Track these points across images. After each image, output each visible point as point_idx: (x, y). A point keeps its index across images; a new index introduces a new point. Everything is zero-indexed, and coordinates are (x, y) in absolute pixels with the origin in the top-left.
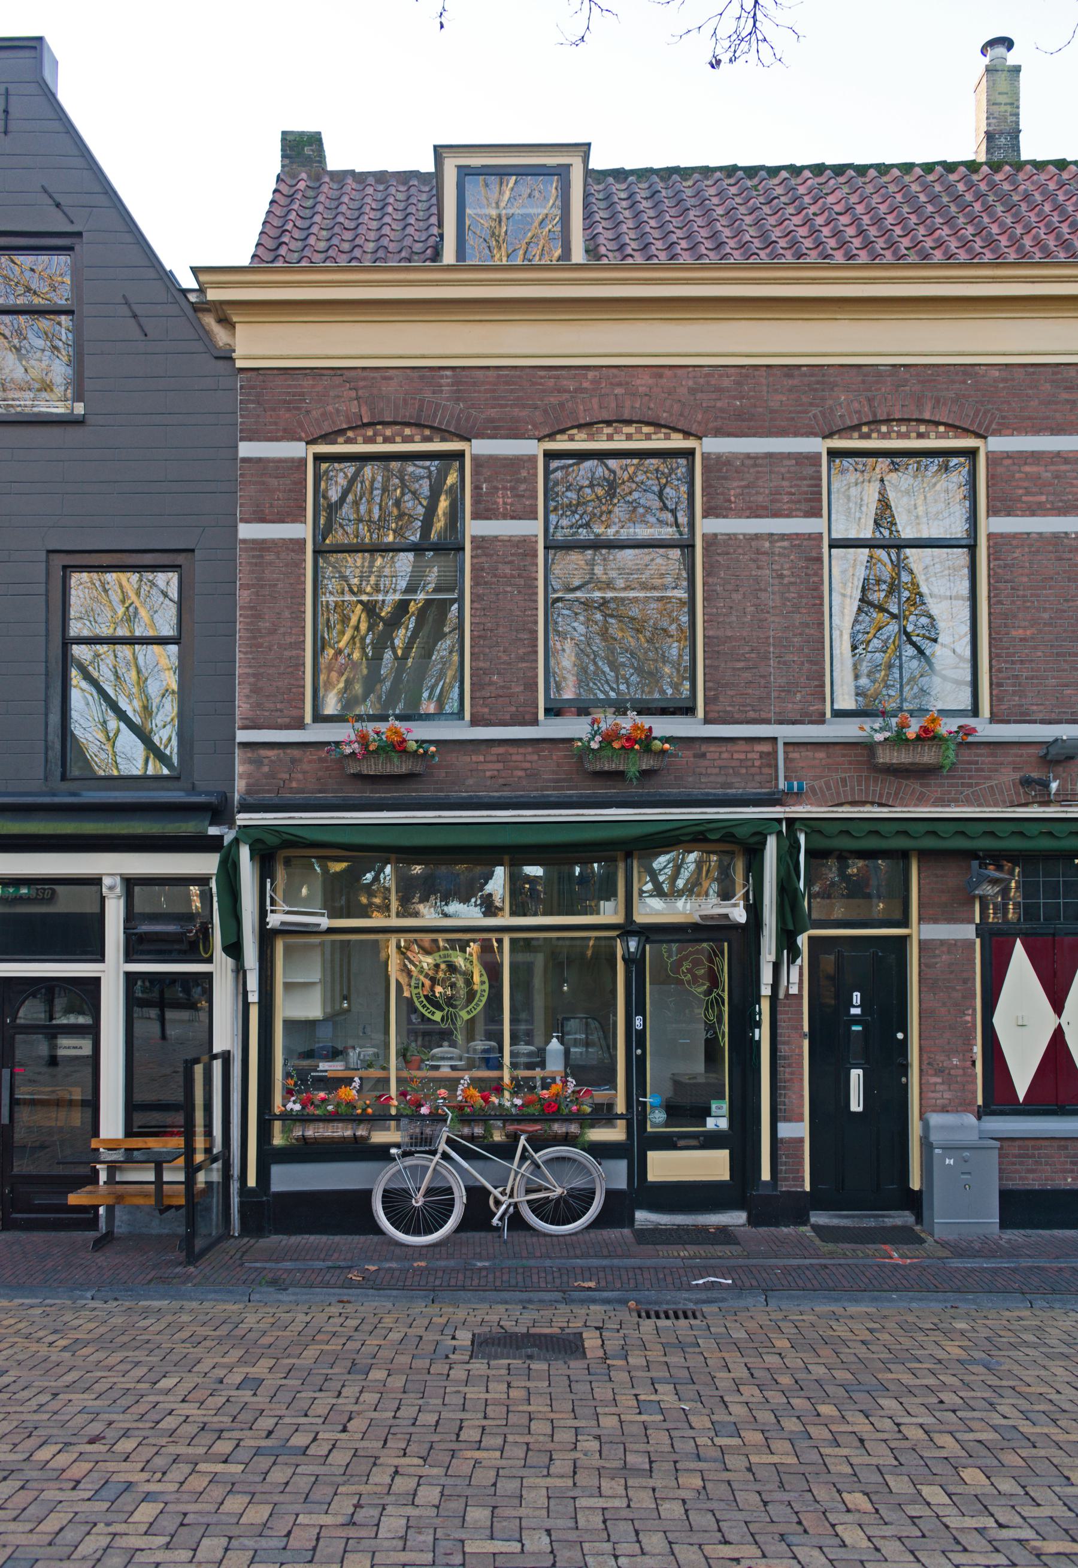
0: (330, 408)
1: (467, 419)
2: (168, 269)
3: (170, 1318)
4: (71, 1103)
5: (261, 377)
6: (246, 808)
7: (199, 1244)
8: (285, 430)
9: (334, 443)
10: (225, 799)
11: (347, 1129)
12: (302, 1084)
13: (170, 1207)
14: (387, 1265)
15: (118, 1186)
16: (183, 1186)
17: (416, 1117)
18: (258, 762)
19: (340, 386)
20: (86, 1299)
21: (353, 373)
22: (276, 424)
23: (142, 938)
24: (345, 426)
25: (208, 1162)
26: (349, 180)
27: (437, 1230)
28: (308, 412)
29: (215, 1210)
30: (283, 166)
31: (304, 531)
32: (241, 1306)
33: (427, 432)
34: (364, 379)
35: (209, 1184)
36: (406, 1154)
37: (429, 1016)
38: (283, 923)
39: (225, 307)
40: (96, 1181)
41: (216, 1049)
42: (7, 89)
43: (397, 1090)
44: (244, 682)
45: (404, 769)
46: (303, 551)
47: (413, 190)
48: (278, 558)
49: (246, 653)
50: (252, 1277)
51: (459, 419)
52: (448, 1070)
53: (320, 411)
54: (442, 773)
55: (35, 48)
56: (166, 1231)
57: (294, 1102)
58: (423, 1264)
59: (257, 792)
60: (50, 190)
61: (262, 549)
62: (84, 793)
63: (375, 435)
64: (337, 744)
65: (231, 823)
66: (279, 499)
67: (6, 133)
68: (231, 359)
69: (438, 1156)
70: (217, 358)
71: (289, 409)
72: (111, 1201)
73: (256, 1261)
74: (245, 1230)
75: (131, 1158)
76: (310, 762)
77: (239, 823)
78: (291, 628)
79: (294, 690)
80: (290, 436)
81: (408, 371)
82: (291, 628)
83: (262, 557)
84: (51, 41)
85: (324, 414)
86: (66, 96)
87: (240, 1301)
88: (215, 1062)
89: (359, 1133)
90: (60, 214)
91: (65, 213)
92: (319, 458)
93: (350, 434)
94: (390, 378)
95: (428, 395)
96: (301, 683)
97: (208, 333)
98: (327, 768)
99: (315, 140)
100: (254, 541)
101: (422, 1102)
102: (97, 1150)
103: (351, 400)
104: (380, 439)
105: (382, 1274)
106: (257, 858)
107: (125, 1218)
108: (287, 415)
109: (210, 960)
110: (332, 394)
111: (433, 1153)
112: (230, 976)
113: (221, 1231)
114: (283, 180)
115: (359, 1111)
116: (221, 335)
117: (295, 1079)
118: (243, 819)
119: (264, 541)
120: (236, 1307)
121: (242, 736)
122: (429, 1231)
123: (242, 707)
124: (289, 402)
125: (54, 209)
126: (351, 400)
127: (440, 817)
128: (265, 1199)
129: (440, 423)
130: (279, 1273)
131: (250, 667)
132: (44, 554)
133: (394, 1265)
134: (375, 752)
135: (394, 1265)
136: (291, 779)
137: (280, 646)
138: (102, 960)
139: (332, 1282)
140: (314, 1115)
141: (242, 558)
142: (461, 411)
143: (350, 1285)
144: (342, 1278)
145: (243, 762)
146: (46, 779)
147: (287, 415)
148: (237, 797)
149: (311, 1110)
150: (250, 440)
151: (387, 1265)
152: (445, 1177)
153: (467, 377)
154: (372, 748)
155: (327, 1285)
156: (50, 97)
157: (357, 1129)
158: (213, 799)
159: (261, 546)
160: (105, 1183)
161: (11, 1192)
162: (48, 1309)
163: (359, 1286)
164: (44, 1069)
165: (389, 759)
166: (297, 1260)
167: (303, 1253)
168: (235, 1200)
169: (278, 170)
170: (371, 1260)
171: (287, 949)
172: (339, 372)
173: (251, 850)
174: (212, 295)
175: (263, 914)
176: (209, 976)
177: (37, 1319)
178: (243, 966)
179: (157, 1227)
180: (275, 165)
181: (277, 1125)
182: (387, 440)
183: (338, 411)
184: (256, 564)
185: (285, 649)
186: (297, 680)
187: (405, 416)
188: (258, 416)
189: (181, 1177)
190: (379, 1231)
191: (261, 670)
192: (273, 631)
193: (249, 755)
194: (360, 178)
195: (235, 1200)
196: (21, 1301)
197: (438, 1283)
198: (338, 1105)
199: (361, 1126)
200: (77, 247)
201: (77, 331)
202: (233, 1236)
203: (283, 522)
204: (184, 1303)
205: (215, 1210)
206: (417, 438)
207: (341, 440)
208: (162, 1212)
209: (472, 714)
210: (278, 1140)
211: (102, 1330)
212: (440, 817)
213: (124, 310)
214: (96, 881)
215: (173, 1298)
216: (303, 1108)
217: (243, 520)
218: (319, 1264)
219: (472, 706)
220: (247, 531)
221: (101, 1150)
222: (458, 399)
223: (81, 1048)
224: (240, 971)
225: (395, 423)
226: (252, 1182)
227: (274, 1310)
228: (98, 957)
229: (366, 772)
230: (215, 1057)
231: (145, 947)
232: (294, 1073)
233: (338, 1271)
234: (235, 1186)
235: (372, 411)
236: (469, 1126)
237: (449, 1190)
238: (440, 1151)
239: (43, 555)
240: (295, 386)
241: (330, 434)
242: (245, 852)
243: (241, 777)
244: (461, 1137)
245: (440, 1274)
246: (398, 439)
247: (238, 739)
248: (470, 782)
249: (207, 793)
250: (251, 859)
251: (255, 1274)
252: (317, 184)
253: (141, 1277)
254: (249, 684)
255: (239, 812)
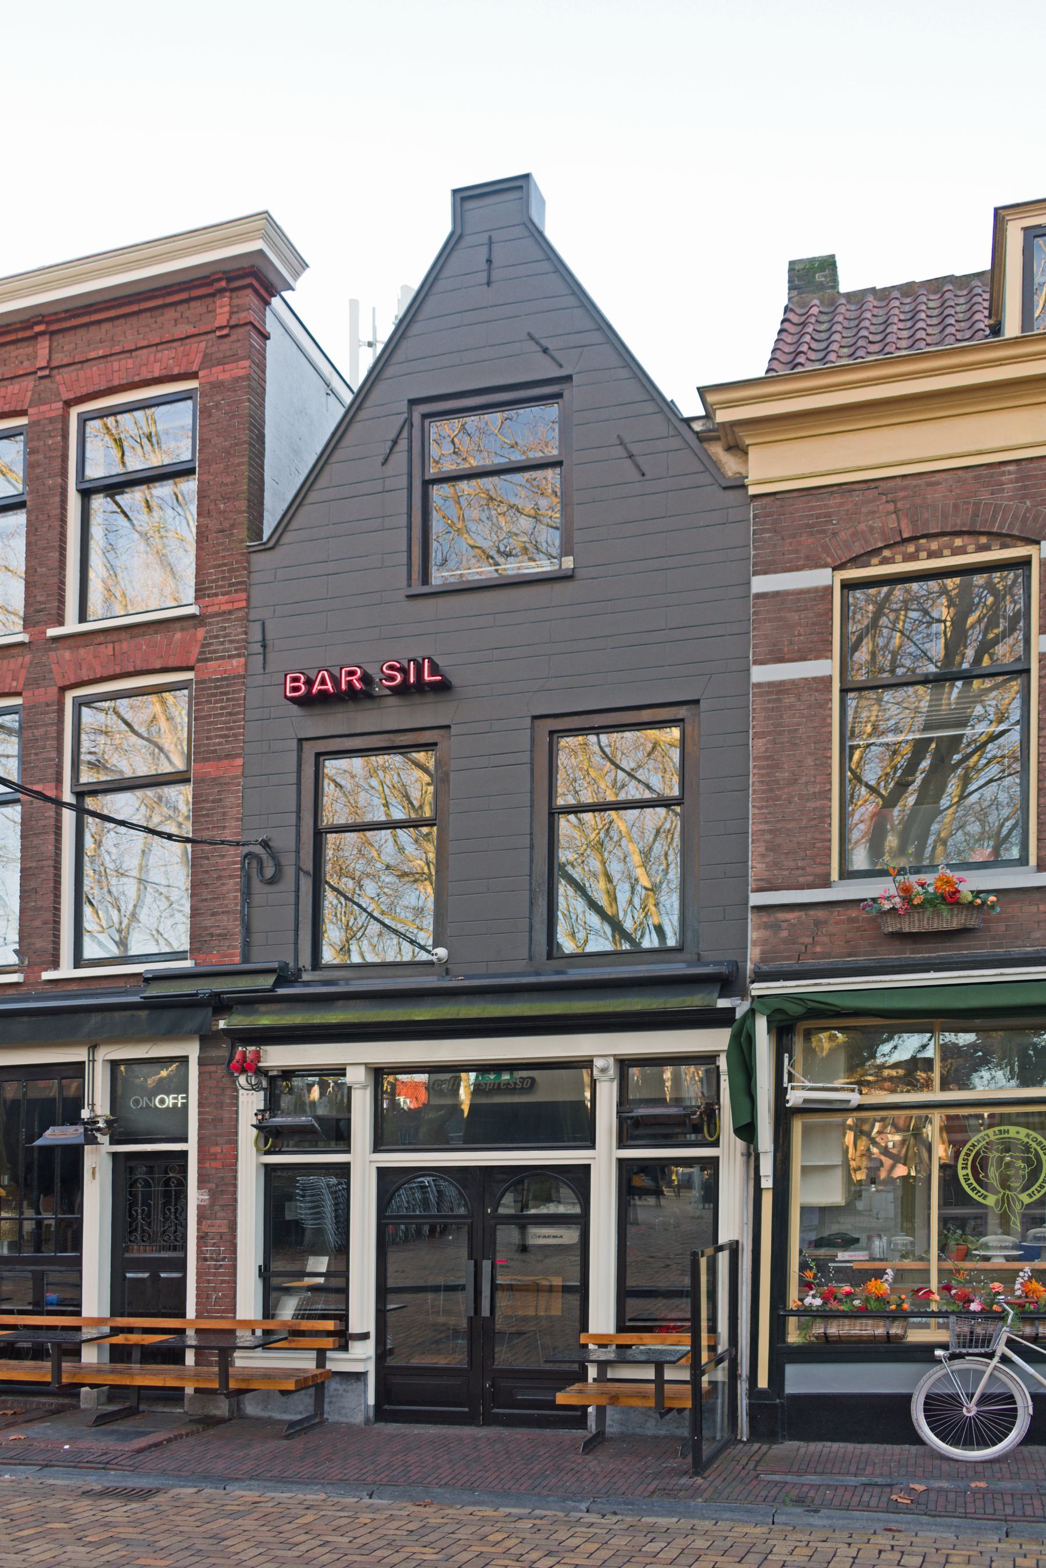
0: (862, 526)
1: (1035, 519)
2: (669, 399)
3: (681, 1542)
4: (551, 1289)
5: (778, 502)
6: (761, 976)
7: (707, 1449)
8: (807, 558)
9: (867, 565)
10: (737, 968)
11: (878, 1327)
12: (822, 1277)
13: (671, 1410)
14: (937, 1484)
15: (609, 1385)
16: (689, 1387)
17: (965, 1314)
18: (776, 927)
19: (874, 500)
20: (581, 1511)
21: (891, 484)
22: (796, 552)
23: (638, 1122)
24: (880, 545)
25: (713, 1364)
26: (870, 298)
27: (994, 1444)
28: (835, 534)
29: (719, 1411)
30: (790, 299)
31: (828, 667)
32: (765, 1529)
33: (983, 540)
34: (904, 488)
35: (713, 1384)
36: (953, 1357)
37: (980, 1200)
38: (806, 1101)
39: (736, 429)
40: (585, 1379)
41: (723, 1238)
42: (490, 238)
43: (939, 1282)
44: (758, 841)
45: (955, 924)
46: (829, 689)
47: (948, 295)
48: (799, 700)
49: (760, 808)
50: (773, 1493)
51: (1025, 519)
52: (1003, 1260)
53: (849, 532)
54: (1001, 928)
55: (521, 187)
56: (663, 1433)
57: (814, 1297)
58: (982, 1484)
59: (773, 960)
60: (537, 336)
61: (779, 692)
62: (571, 971)
63: (917, 551)
64: (874, 900)
65: (743, 993)
66: (800, 635)
67: (488, 284)
68: (744, 487)
69: (996, 1359)
70: (725, 488)
71: (811, 534)
72: (603, 1401)
73: (774, 1473)
74: (755, 1434)
75: (624, 1355)
76: (837, 923)
77: (754, 993)
78: (815, 777)
79: (818, 845)
80: (814, 563)
81: (960, 472)
82: (815, 777)
83: (779, 700)
84: (538, 178)
85: (855, 534)
86: (554, 232)
87: (763, 1523)
88: (720, 1254)
89: (893, 1331)
90: (549, 358)
91: (553, 358)
92: (847, 586)
93: (886, 553)
94: (938, 483)
95: (985, 496)
96: (827, 836)
97: (716, 465)
98: (858, 929)
99: (828, 265)
100: (770, 684)
101: (971, 1297)
102: (585, 1346)
103: (889, 513)
104: (923, 554)
105: (933, 1495)
106: (774, 1031)
107: (616, 1417)
108: (810, 541)
109: (716, 1144)
110: (864, 510)
111: (990, 1356)
112: (740, 1160)
113: (726, 1436)
114: (792, 310)
115: (893, 1307)
116: (730, 464)
117: (814, 1271)
118: (758, 989)
119: (782, 683)
120: (758, 1530)
121: (756, 899)
122: (984, 1444)
123: (756, 868)
124: (812, 526)
125: (541, 355)
126: (889, 513)
127: (1002, 974)
128: (778, 1401)
129: (1001, 527)
130: (805, 1489)
131: (766, 823)
132: (529, 719)
133: (945, 1484)
134: (921, 906)
135: (945, 1484)
136: (814, 943)
137: (801, 797)
138: (593, 1146)
139: (873, 1502)
140: (838, 1311)
141: (754, 703)
142: (1028, 510)
143: (895, 1508)
144: (884, 1499)
145: (758, 928)
146: (531, 958)
147: (810, 541)
148: (750, 966)
149: (834, 1305)
150: (765, 573)
151: (937, 1484)
152: (1004, 1384)
153: (1035, 469)
154: (916, 902)
155: (867, 1508)
156: (537, 236)
157: (891, 1327)
158: (724, 969)
159: (779, 688)
160: (595, 1380)
161: (492, 1386)
162: (538, 1522)
163: (907, 1510)
164: (517, 1256)
165: (938, 914)
166: (823, 1473)
167: (829, 1466)
168: (743, 1402)
169: (785, 302)
170: (914, 1477)
171: (806, 1130)
172: (873, 485)
173: (768, 1022)
174: (722, 416)
175: (780, 1093)
176: (716, 1160)
177: (528, 1535)
178: (756, 1149)
179: (652, 1428)
180: (781, 296)
181: (792, 1322)
182: (931, 555)
183: (872, 529)
184: (772, 710)
185: (808, 800)
186: (822, 833)
187: (956, 525)
188: (775, 546)
189: (686, 1375)
190: (917, 1440)
191: (779, 826)
192: (794, 782)
193: (765, 919)
194: (883, 295)
195: (743, 1402)
196: (508, 1510)
197: (1009, 1510)
198: (867, 1300)
199: (896, 1323)
200: (566, 394)
201: (564, 481)
202: (741, 1441)
203: (805, 659)
204: (696, 1522)
205: (719, 1411)
206: (971, 548)
207: (875, 561)
208: (662, 1416)
209: (1039, 858)
210: (793, 1337)
211: (604, 1554)
212: (1002, 974)
213: (620, 451)
214: (587, 1063)
215: (682, 1515)
216: (825, 1303)
217: (755, 663)
218: (851, 1480)
219: (1039, 848)
220: (760, 674)
221: (591, 1346)
222: (1024, 497)
223: (561, 1237)
224: (752, 1156)
225: (943, 534)
226: (763, 1383)
227: (807, 1538)
228: (589, 1144)
229: (907, 930)
230: (721, 1249)
231: (641, 1131)
232: (812, 1264)
233: (877, 1490)
234: (743, 1387)
235: (914, 523)
236: (1032, 1325)
237: (1010, 1398)
238: (998, 1354)
239: (528, 722)
240: (820, 507)
241: (862, 555)
242: (761, 1024)
243: (755, 943)
244: (1022, 1337)
245: (1008, 1499)
246: (946, 552)
247: (751, 903)
248: (1037, 934)
249: (716, 963)
250: (769, 1032)
251: (776, 1490)
252: (832, 309)
253: (642, 1488)
254: (765, 841)
255: (753, 982)
